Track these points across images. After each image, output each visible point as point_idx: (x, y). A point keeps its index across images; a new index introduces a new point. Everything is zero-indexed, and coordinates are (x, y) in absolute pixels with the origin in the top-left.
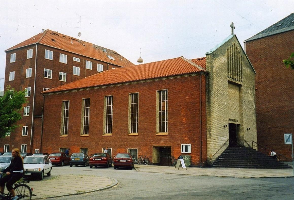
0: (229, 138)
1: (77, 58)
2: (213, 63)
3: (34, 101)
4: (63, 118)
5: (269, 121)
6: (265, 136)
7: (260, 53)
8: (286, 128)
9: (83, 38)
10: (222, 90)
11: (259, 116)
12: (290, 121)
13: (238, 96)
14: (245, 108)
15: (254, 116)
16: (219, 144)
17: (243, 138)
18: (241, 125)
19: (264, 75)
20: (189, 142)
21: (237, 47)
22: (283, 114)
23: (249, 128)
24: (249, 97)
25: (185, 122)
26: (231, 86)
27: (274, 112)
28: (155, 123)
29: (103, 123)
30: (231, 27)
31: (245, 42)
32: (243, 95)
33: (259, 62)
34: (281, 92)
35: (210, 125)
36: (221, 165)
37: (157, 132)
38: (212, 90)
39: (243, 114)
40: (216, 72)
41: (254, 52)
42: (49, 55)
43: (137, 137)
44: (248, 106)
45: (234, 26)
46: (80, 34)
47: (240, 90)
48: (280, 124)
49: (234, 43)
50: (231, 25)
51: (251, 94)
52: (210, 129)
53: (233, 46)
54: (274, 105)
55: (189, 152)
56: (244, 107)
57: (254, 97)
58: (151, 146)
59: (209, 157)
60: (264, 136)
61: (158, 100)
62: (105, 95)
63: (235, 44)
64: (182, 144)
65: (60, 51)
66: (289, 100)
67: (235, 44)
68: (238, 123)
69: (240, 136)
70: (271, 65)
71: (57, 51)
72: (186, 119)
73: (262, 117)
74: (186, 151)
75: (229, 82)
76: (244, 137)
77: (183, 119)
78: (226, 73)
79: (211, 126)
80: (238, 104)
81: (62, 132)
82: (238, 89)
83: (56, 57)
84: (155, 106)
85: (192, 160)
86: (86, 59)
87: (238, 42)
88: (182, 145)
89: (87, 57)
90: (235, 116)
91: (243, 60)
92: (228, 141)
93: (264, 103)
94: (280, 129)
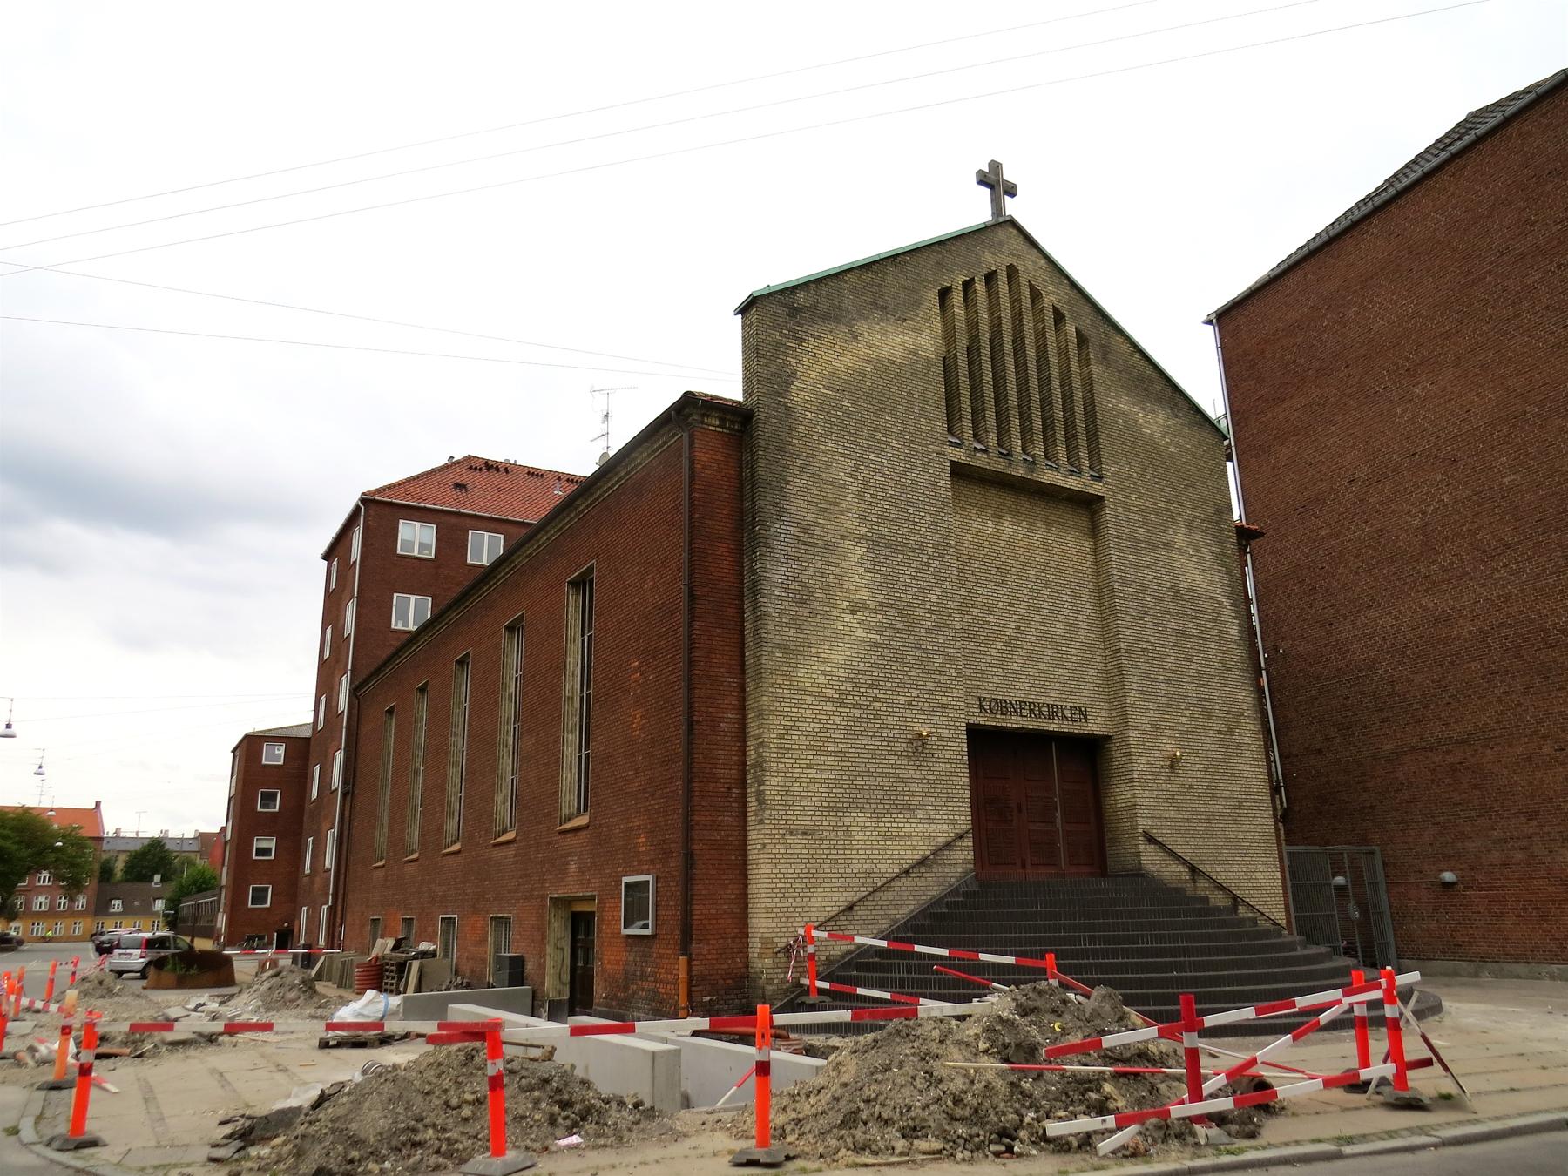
5: (1385, 715)
6: (1372, 807)
8: (1485, 746)
12: (1500, 701)
13: (1085, 564)
17: (1133, 820)
21: (1032, 287)
22: (1452, 663)
26: (973, 492)
27: (1403, 654)
28: (557, 762)
30: (981, 182)
32: (1117, 559)
34: (1425, 535)
37: (565, 811)
38: (780, 513)
39: (1120, 669)
44: (1173, 624)
45: (1008, 176)
47: (1094, 531)
48: (1447, 725)
52: (760, 765)
53: (990, 278)
54: (1396, 618)
57: (1227, 573)
58: (543, 898)
63: (1012, 271)
64: (625, 879)
65: (468, 521)
66: (1475, 569)
68: (1095, 726)
69: (1116, 809)
70: (1350, 396)
71: (453, 520)
73: (1347, 698)
75: (959, 472)
76: (1141, 812)
80: (1086, 608)
82: (1083, 522)
87: (1043, 262)
93: (1344, 616)
94: (1449, 759)
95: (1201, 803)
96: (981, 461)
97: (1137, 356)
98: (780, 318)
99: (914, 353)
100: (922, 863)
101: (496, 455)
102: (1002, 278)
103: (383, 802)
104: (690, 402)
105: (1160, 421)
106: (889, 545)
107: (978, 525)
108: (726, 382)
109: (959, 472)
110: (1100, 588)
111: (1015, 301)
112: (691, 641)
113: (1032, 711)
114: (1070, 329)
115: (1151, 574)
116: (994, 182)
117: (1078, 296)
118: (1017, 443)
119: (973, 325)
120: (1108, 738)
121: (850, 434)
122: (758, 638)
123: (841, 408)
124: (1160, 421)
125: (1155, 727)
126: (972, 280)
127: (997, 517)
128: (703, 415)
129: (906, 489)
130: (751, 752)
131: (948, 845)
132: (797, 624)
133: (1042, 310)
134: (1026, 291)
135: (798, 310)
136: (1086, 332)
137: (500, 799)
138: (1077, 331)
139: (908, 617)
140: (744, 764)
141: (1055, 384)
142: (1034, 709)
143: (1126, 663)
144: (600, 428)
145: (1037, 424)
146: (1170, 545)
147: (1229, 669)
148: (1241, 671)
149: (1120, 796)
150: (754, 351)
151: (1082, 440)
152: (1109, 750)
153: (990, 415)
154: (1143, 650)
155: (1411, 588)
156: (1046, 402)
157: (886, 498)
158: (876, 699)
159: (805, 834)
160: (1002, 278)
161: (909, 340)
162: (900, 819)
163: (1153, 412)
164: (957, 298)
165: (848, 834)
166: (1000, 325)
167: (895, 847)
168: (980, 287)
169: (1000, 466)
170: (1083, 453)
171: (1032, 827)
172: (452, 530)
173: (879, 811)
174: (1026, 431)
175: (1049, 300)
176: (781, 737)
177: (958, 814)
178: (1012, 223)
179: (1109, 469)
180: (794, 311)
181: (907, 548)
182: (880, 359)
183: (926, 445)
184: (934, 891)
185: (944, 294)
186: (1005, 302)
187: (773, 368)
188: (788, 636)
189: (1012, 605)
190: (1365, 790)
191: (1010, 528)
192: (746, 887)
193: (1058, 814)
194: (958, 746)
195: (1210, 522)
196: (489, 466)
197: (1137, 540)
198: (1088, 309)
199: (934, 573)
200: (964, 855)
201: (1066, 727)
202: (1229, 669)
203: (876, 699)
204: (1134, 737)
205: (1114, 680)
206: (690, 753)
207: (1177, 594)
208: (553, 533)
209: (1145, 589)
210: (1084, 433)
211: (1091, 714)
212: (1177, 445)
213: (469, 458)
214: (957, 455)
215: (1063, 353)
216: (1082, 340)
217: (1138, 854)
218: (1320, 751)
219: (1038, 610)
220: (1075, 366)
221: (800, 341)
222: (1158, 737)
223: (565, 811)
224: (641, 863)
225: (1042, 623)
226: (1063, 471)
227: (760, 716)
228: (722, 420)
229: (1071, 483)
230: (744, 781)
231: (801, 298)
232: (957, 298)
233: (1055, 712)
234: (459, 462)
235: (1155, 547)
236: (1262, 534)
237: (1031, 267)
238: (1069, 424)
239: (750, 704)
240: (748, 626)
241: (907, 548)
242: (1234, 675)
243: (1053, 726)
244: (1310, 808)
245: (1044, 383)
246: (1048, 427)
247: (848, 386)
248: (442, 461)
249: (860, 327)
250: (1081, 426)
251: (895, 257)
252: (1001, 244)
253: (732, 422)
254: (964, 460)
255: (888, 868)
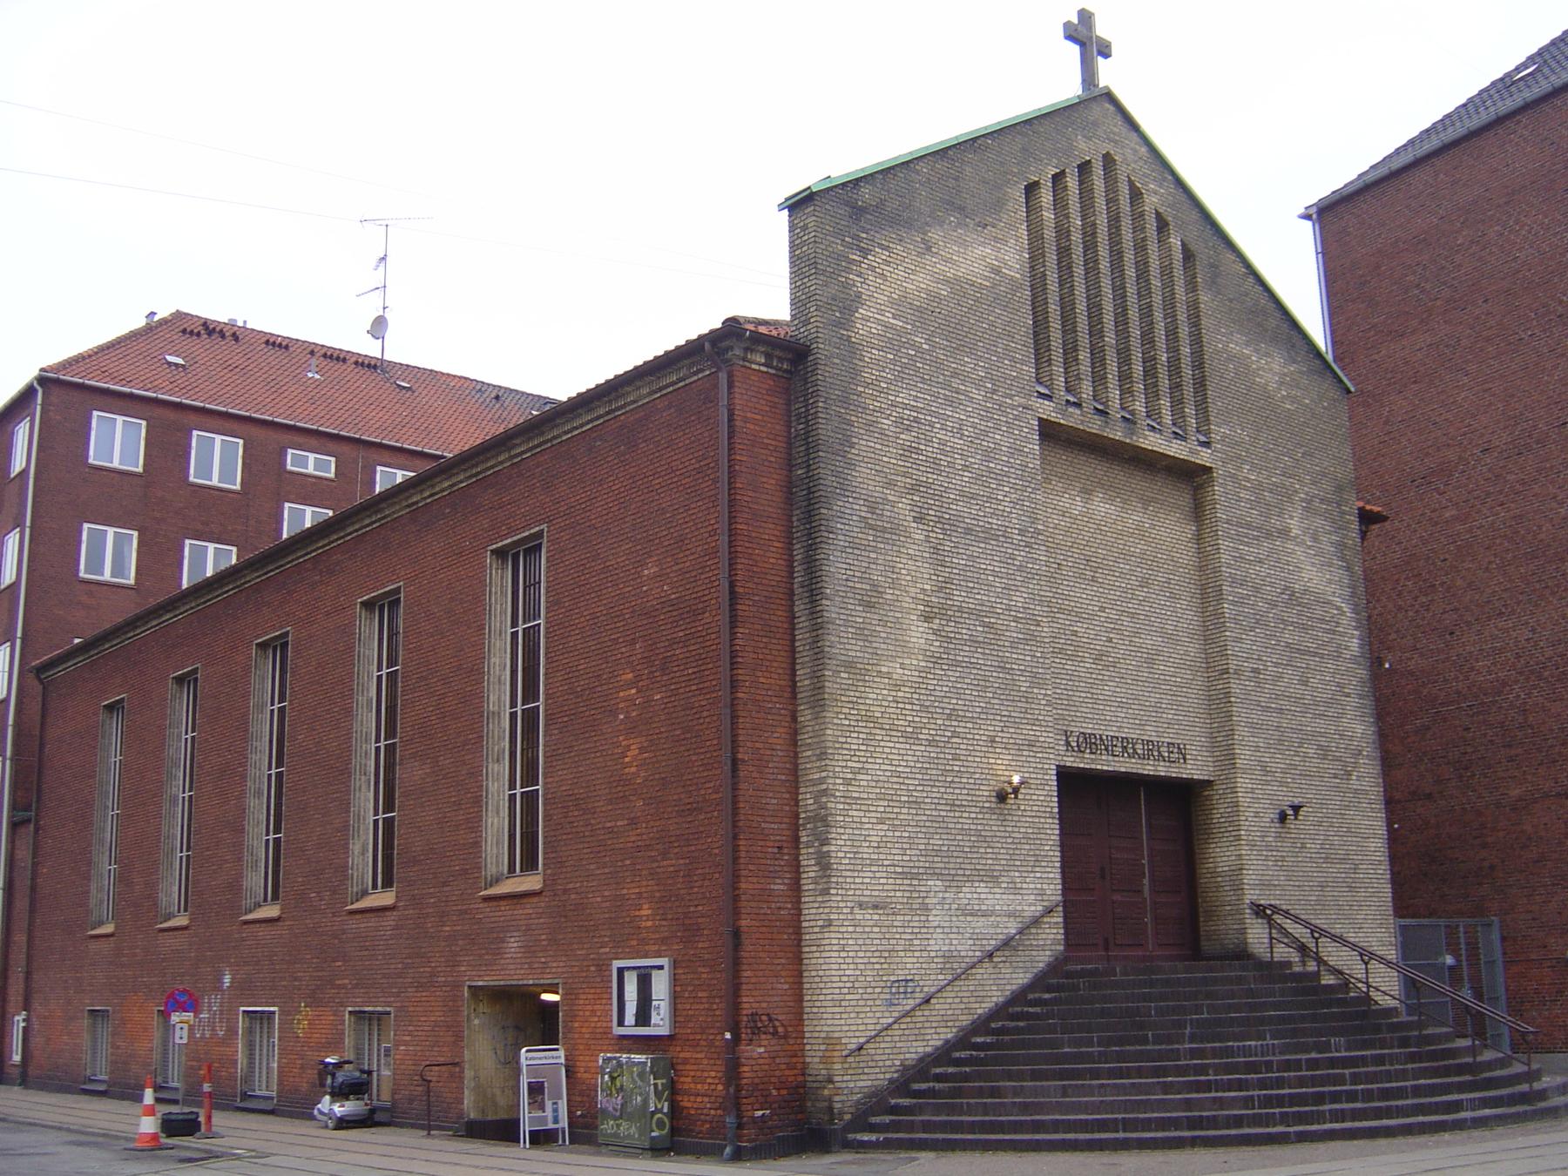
0: (1066, 889)
1: (312, 457)
2: (848, 270)
3: (11, 721)
4: (105, 816)
7: (1414, 273)
9: (401, 349)
10: (973, 497)
11: (1445, 720)
13: (1186, 555)
14: (1243, 647)
15: (1350, 714)
16: (937, 944)
17: (1238, 888)
18: (1219, 788)
19: (1449, 416)
20: (664, 941)
21: (1131, 184)
23: (1296, 809)
24: (1303, 564)
25: (636, 775)
26: (1062, 457)
29: (242, 831)
30: (1069, 37)
31: (1314, 210)
32: (1226, 549)
33: (1413, 333)
35: (822, 781)
36: (1354, 1075)
37: (491, 870)
39: (1228, 694)
40: (894, 341)
41: (1378, 267)
42: (216, 461)
43: (390, 920)
44: (1288, 637)
45: (1102, 30)
46: (378, 327)
47: (1199, 512)
49: (1107, 147)
50: (1067, 25)
51: (1315, 540)
52: (824, 819)
53: (1084, 168)
54: (1533, 630)
55: (660, 1023)
56: (1239, 640)
57: (1348, 569)
58: (457, 986)
59: (813, 1059)
60: (1486, 864)
61: (496, 624)
62: (257, 637)
63: (1108, 160)
64: (617, 964)
65: (193, 418)
67: (1108, 160)
68: (1193, 770)
69: (1215, 874)
70: (1488, 339)
71: (171, 415)
72: (642, 750)
74: (643, 1017)
75: (1050, 433)
76: (1249, 878)
77: (628, 748)
78: (1013, 360)
79: (825, 792)
80: (1184, 615)
81: (101, 902)
82: (1185, 500)
83: (168, 446)
84: (475, 672)
85: (688, 1093)
86: (375, 456)
87: (1144, 150)
88: (621, 971)
89: (380, 446)
90: (1147, 722)
91: (1213, 282)
92: (1058, 918)
93: (1468, 624)
95: (1310, 864)
96: (1073, 419)
97: (1251, 279)
98: (836, 220)
99: (997, 271)
100: (1007, 943)
101: (218, 313)
102: (1098, 170)
103: (101, 841)
104: (733, 328)
105: (1276, 367)
106: (968, 531)
107: (1065, 502)
108: (768, 299)
109: (1050, 433)
110: (1203, 588)
111: (1111, 201)
112: (733, 655)
113: (1124, 748)
114: (1175, 242)
115: (1264, 571)
116: (1086, 39)
117: (1183, 198)
118: (1115, 394)
119: (1062, 232)
120: (1209, 783)
121: (923, 381)
122: (819, 654)
123: (913, 346)
124: (1276, 367)
125: (1265, 769)
126: (1063, 172)
127: (1087, 492)
128: (746, 350)
129: (988, 455)
130: (808, 801)
131: (1036, 922)
132: (863, 634)
133: (1142, 215)
134: (1124, 190)
135: (863, 210)
136: (1193, 247)
137: (355, 847)
138: (1183, 244)
139: (989, 625)
140: (797, 816)
141: (1158, 315)
142: (1127, 746)
143: (1235, 688)
144: (376, 278)
145: (1138, 369)
146: (1284, 533)
147: (1348, 695)
148: (1361, 697)
149: (1220, 857)
150: (803, 263)
151: (1188, 390)
152: (1209, 798)
153: (1084, 356)
154: (1255, 671)
155: (1553, 593)
156: (1148, 338)
157: (966, 468)
158: (955, 734)
159: (876, 907)
160: (1098, 170)
161: (988, 256)
162: (982, 888)
163: (1267, 355)
164: (1046, 196)
165: (926, 908)
166: (1094, 234)
167: (980, 924)
168: (1072, 182)
169: (1094, 426)
170: (1190, 410)
171: (1117, 897)
172: (170, 424)
173: (953, 881)
174: (1125, 377)
175: (1151, 202)
176: (847, 782)
177: (1052, 887)
178: (1109, 96)
179: (1218, 431)
180: (858, 212)
181: (989, 535)
182: (957, 279)
183: (1011, 397)
184: (1021, 978)
185: (1031, 189)
186: (1100, 202)
187: (833, 290)
188: (854, 650)
189: (1102, 609)
190: (1484, 846)
191: (1102, 507)
192: (800, 974)
193: (1146, 881)
194: (1043, 799)
195: (1329, 502)
196: (210, 329)
197: (1249, 526)
198: (1195, 215)
199: (1020, 568)
200: (1052, 936)
201: (1162, 770)
202: (1348, 695)
203: (955, 734)
204: (1243, 783)
205: (1219, 708)
206: (735, 802)
207: (1292, 597)
208: (461, 479)
209: (1257, 589)
210: (1190, 384)
211: (1192, 751)
212: (1294, 400)
213: (179, 316)
214: (1047, 410)
215: (1167, 271)
216: (1188, 255)
217: (1243, 932)
218: (1429, 796)
219: (1133, 616)
220: (1180, 292)
221: (865, 252)
222: (1267, 783)
223: (491, 870)
224: (643, 942)
225: (1136, 634)
226: (1168, 433)
227: (822, 756)
228: (768, 356)
229: (1176, 450)
230: (797, 839)
231: (866, 194)
232: (1046, 196)
233: (1152, 750)
234: (164, 322)
235: (1269, 535)
236: (1385, 519)
237: (1130, 157)
238: (1174, 367)
239: (805, 737)
240: (802, 636)
241: (989, 535)
242: (1354, 701)
243: (1149, 768)
244: (1425, 873)
245: (1146, 313)
246: (1150, 372)
247: (922, 313)
248: (140, 322)
249: (935, 235)
250: (1187, 372)
251: (974, 140)
252: (1095, 124)
253: (780, 359)
254: (1054, 417)
255: (966, 949)
